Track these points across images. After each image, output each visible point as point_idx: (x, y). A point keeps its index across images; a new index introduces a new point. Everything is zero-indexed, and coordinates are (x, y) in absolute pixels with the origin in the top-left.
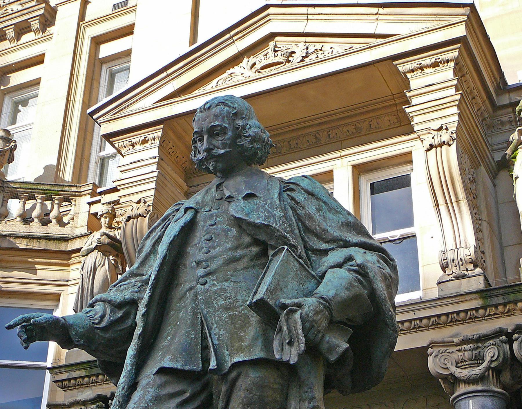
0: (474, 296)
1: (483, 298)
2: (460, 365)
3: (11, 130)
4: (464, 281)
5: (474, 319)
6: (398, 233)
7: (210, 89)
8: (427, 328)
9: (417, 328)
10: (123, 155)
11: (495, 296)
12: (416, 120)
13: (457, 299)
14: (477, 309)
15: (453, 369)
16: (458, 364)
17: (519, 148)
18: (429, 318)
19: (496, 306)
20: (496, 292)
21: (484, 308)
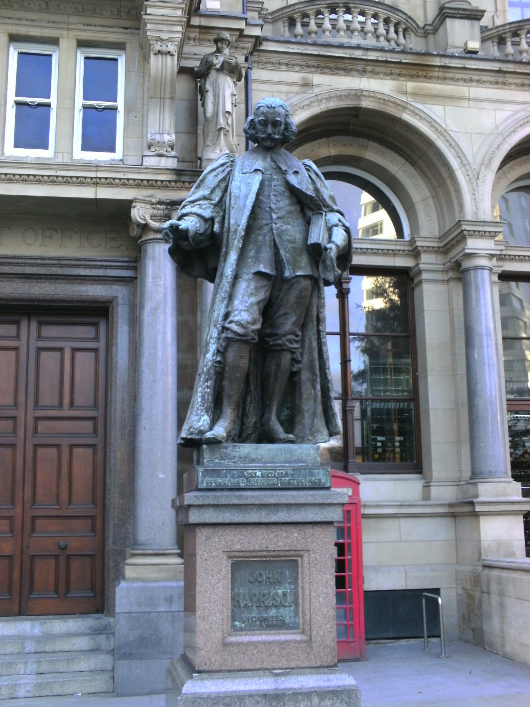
0: (166, 172)
1: (177, 175)
2: (153, 218)
3: (149, 21)
4: (163, 159)
5: (166, 187)
6: (105, 104)
7: (270, 82)
8: (131, 186)
9: (124, 185)
10: (183, 56)
11: (185, 175)
12: (149, 26)
13: (158, 171)
14: (170, 182)
15: (150, 221)
16: (153, 217)
17: (524, 222)
18: (134, 180)
19: (184, 182)
20: (186, 173)
21: (176, 182)
